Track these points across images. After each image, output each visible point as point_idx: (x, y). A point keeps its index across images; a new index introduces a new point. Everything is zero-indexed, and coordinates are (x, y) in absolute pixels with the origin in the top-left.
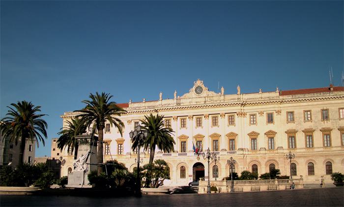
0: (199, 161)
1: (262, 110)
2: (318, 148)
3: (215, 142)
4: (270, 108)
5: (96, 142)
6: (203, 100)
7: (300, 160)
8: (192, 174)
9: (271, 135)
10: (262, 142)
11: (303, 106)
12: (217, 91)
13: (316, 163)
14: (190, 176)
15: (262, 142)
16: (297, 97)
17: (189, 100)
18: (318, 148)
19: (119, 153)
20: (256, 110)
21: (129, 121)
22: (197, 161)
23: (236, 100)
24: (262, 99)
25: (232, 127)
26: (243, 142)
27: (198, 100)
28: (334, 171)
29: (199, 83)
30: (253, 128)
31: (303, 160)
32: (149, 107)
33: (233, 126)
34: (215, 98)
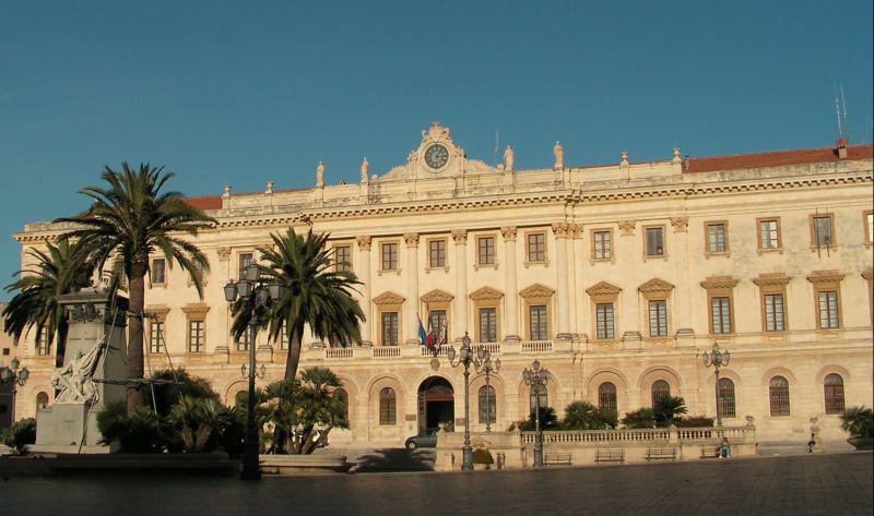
0: (439, 374)
1: (227, 245)
6: (451, 185)
7: (746, 369)
10: (631, 314)
11: (753, 204)
15: (631, 314)
16: (753, 176)
17: (405, 188)
19: (194, 348)
21: (224, 249)
23: (552, 188)
24: (631, 185)
27: (434, 186)
31: (755, 369)
33: (542, 267)
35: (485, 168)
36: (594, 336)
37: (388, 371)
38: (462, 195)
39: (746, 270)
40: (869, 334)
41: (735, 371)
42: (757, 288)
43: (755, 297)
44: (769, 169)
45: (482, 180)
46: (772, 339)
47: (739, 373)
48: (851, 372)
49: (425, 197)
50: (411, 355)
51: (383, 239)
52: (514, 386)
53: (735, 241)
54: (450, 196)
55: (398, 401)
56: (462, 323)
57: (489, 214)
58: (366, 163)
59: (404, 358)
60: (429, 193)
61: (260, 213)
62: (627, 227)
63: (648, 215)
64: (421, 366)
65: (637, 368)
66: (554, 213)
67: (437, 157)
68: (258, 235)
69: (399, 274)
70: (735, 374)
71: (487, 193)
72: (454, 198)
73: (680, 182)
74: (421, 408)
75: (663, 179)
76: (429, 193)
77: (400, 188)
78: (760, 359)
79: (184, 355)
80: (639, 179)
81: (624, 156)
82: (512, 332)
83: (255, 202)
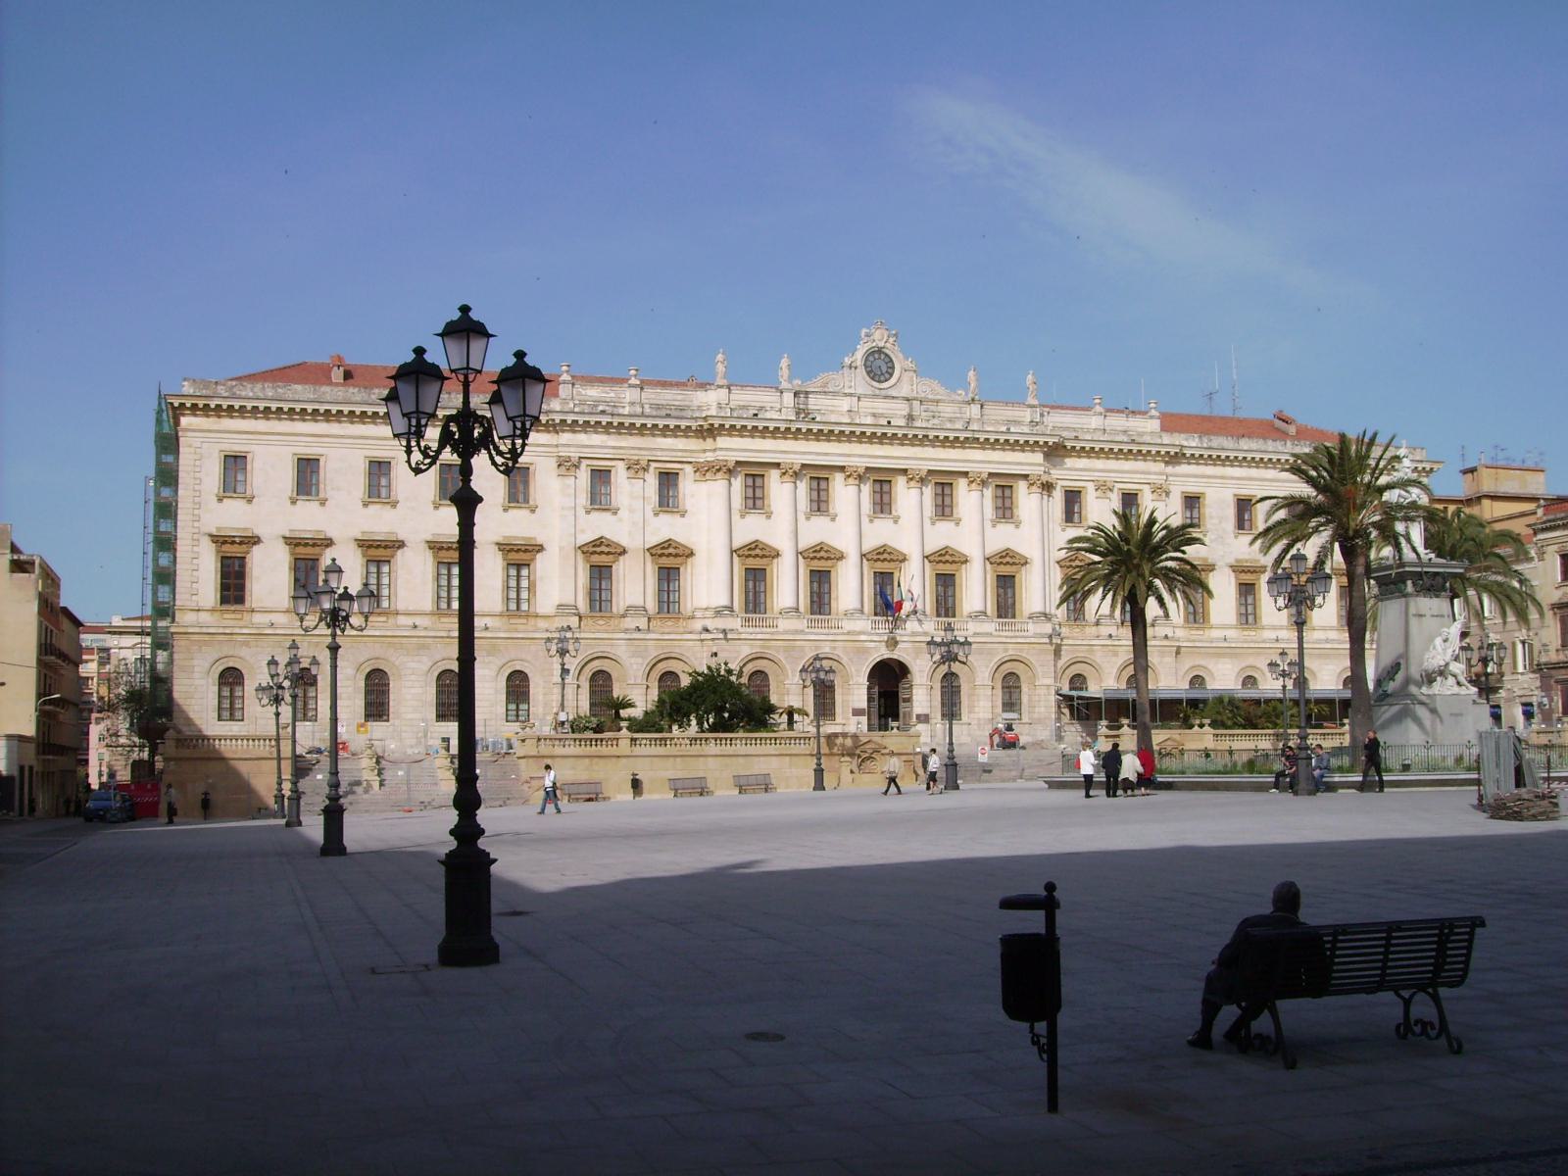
0: (895, 655)
1: (574, 454)
2: (1324, 629)
3: (946, 585)
4: (307, 437)
5: (1368, 571)
6: (902, 409)
7: (1220, 666)
8: (864, 705)
9: (670, 562)
10: (634, 584)
11: (1232, 478)
12: (953, 380)
13: (1212, 675)
14: (857, 712)
15: (634, 584)
16: (358, 398)
17: (845, 404)
18: (1324, 629)
19: (513, 606)
20: (1086, 475)
21: (568, 460)
22: (884, 653)
23: (1026, 430)
24: (1106, 437)
25: (1005, 528)
26: (709, 584)
27: (881, 406)
28: (363, 721)
29: (864, 331)
30: (752, 528)
31: (1229, 666)
32: (658, 407)
33: (1010, 527)
34: (947, 410)
35: (941, 392)
36: (1063, 617)
37: (827, 650)
38: (918, 424)
39: (1222, 553)
40: (476, 635)
41: (1210, 667)
42: (1233, 575)
43: (1230, 583)
44: (1177, 434)
45: (941, 407)
46: (1246, 633)
47: (1213, 670)
48: (1318, 675)
49: (869, 420)
50: (857, 629)
51: (595, 462)
52: (987, 674)
53: (1211, 518)
54: (902, 422)
55: (1025, 688)
56: (914, 583)
57: (768, 444)
58: (784, 363)
59: (849, 633)
60: (874, 415)
61: (621, 411)
62: (637, 468)
63: (1127, 477)
64: (872, 645)
65: (1114, 659)
66: (1032, 462)
67: (879, 367)
68: (623, 444)
69: (1017, 527)
70: (1210, 671)
71: (949, 426)
72: (907, 426)
73: (1159, 441)
74: (870, 700)
75: (1141, 434)
76: (874, 415)
77: (835, 402)
78: (1235, 655)
79: (501, 615)
80: (1115, 432)
81: (633, 372)
82: (1038, 607)
83: (612, 395)
